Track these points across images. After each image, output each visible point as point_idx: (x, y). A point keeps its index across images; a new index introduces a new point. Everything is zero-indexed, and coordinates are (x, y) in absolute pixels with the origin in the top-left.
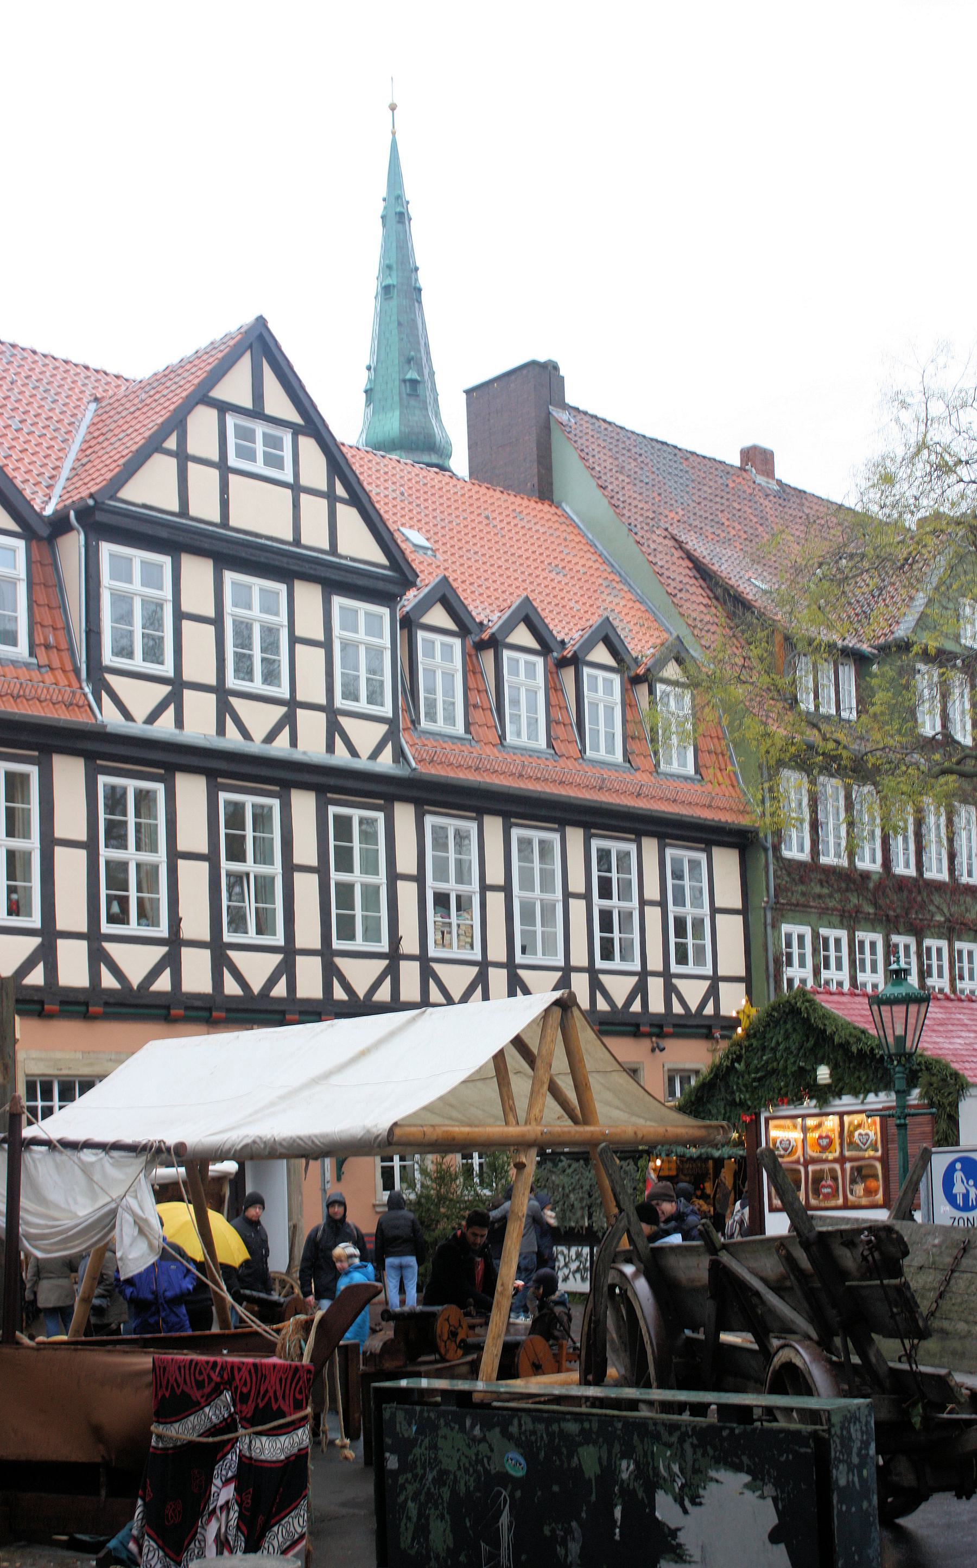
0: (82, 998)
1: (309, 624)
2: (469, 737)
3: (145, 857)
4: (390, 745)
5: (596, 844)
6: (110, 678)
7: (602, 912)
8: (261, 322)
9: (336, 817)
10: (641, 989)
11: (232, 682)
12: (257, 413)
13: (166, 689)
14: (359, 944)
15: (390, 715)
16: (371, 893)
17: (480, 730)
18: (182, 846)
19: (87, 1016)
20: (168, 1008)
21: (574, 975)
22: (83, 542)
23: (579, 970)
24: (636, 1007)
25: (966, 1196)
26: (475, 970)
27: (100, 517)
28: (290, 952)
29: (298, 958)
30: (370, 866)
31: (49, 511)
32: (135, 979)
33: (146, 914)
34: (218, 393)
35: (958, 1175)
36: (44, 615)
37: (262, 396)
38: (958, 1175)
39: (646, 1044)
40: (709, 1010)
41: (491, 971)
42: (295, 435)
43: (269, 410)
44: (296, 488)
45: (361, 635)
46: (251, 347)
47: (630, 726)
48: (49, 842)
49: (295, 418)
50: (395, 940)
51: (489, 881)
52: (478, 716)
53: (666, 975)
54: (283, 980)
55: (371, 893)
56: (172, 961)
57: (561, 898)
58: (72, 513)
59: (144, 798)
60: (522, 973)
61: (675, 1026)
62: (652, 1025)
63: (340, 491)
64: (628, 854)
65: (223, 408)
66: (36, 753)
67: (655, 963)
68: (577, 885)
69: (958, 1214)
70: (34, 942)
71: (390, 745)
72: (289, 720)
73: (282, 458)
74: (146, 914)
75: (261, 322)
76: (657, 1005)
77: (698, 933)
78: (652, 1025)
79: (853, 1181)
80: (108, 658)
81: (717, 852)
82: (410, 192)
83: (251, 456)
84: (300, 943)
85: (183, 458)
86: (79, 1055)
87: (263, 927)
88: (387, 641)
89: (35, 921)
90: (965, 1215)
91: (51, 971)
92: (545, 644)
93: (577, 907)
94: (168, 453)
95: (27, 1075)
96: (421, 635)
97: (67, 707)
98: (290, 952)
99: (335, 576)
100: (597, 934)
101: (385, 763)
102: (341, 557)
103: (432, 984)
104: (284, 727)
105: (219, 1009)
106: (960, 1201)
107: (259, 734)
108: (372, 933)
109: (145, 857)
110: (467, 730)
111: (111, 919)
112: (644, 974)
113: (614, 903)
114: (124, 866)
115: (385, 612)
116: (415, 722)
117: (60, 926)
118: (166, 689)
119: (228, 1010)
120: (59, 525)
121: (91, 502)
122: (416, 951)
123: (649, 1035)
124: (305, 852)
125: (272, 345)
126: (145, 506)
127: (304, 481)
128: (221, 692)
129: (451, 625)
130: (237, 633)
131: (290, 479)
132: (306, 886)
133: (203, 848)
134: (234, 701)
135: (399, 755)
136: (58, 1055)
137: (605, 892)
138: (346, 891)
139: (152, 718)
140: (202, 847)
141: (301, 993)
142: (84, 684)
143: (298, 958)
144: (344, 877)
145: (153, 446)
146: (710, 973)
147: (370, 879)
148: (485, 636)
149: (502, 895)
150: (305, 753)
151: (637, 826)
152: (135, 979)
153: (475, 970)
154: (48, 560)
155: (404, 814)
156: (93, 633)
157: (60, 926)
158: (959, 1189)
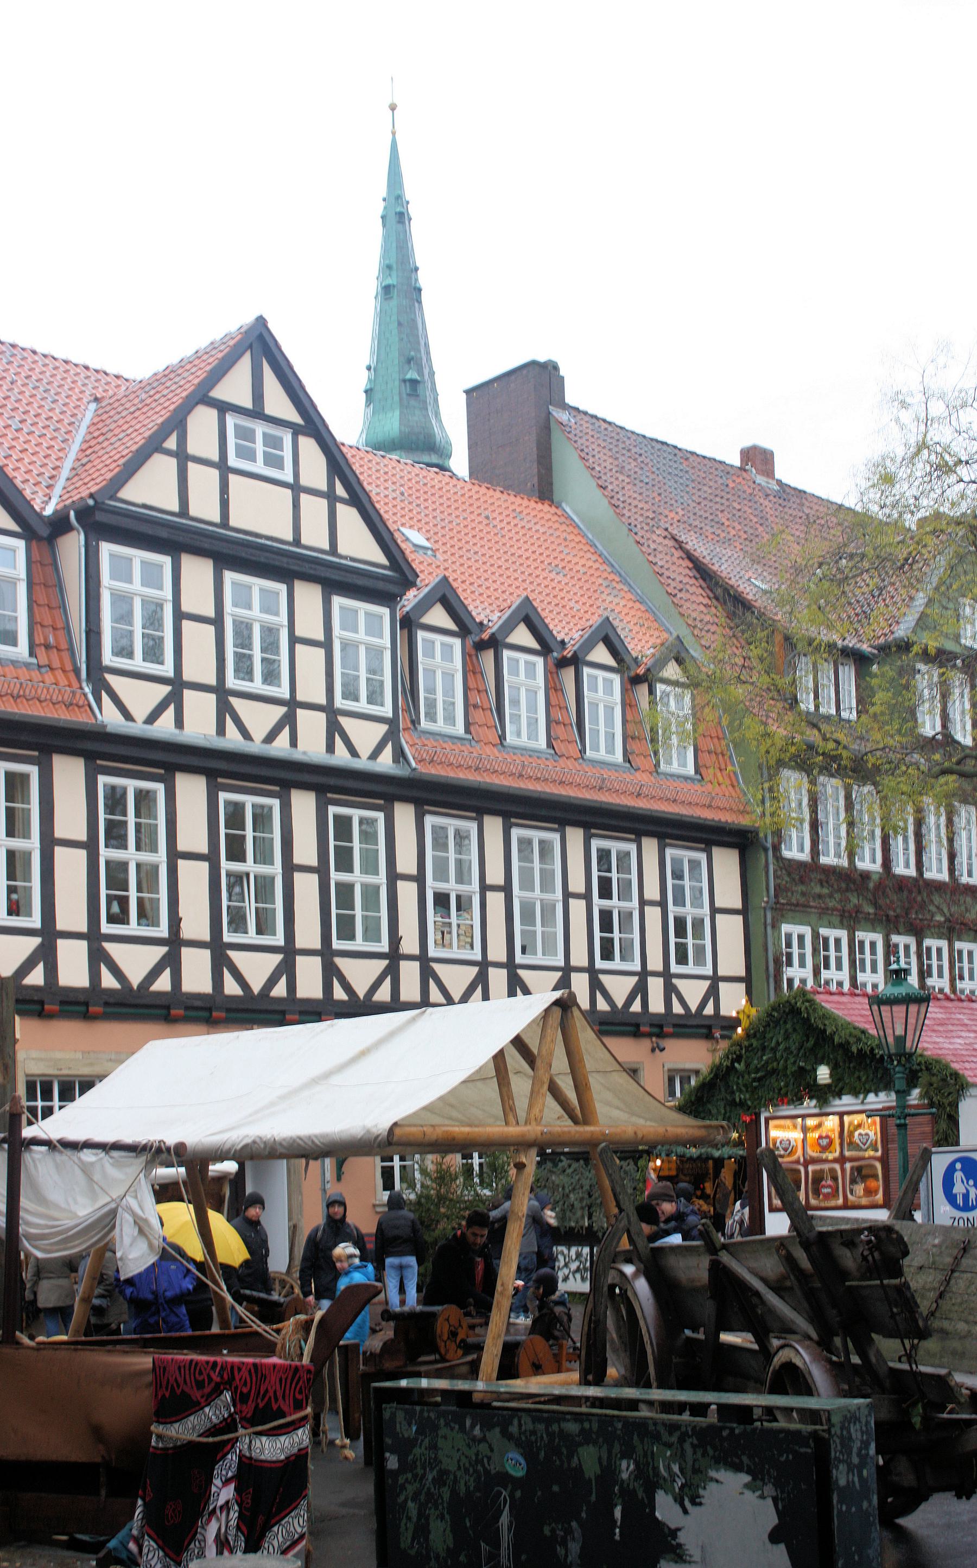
0: (82, 998)
1: (309, 624)
2: (469, 737)
3: (145, 857)
4: (390, 745)
5: (596, 844)
6: (110, 678)
7: (602, 912)
8: (261, 322)
9: (336, 817)
10: (641, 989)
11: (232, 682)
12: (257, 413)
13: (166, 689)
14: (359, 944)
15: (390, 715)
16: (371, 893)
17: (480, 730)
18: (182, 846)
19: (87, 1016)
20: (168, 1008)
21: (574, 975)
22: (83, 542)
23: (579, 970)
24: (636, 1007)
25: (966, 1196)
26: (475, 970)
27: (100, 517)
28: (290, 952)
29: (298, 958)
30: (370, 866)
31: (49, 511)
32: (135, 979)
33: (146, 914)
34: (218, 393)
35: (958, 1175)
36: (44, 615)
37: (262, 396)
38: (958, 1175)
39: (646, 1044)
40: (709, 1010)
41: (491, 971)
42: (295, 435)
43: (269, 410)
44: (296, 488)
45: (361, 635)
46: (251, 347)
47: (630, 726)
48: (49, 842)
49: (295, 418)
50: (395, 940)
51: (489, 881)
52: (478, 716)
53: (666, 975)
54: (283, 980)
55: (371, 893)
56: (172, 961)
57: (561, 898)
58: (72, 513)
59: (144, 798)
60: (522, 973)
61: (675, 1026)
62: (652, 1025)
63: (340, 491)
64: (628, 854)
65: (223, 408)
66: (36, 753)
67: (655, 963)
68: (577, 885)
69: (958, 1214)
70: (34, 942)
71: (390, 745)
72: (289, 720)
73: (282, 458)
74: (146, 914)
75: (261, 322)
76: (657, 1005)
77: (698, 933)
78: (652, 1025)
79: (853, 1181)
80: (108, 658)
81: (717, 852)
82: (410, 192)
83: (251, 456)
84: (300, 943)
85: (183, 458)
86: (79, 1055)
87: (263, 927)
88: (387, 641)
89: (35, 921)
90: (965, 1215)
91: (51, 971)
92: (545, 644)
93: (577, 907)
94: (168, 453)
95: (27, 1075)
96: (421, 635)
97: (67, 707)
98: (290, 952)
99: (335, 576)
100: (597, 934)
101: (385, 763)
102: (341, 557)
103: (432, 984)
104: (284, 727)
105: (219, 1009)
106: (960, 1201)
107: (259, 734)
108: (372, 933)
109: (145, 857)
110: (467, 730)
111: (111, 919)
112: (644, 974)
113: (614, 903)
114: (124, 866)
115: (385, 612)
116: (415, 722)
117: (60, 926)
118: (166, 689)
119: (228, 1010)
120: (59, 525)
121: (91, 502)
122: (416, 951)
123: (649, 1035)
124: (305, 852)
125: (272, 345)
126: (145, 506)
127: (304, 481)
128: (221, 692)
129: (451, 625)
130: (237, 633)
131: (290, 479)
132: (306, 886)
133: (203, 848)
134: (234, 701)
135: (399, 755)
136: (58, 1055)
137: (605, 892)
138: (346, 891)
139: (152, 718)
140: (202, 847)
141: (301, 993)
142: (84, 684)
143: (298, 958)
144: (344, 877)
145: (153, 446)
146: (710, 973)
147: (370, 879)
148: (485, 636)
149: (502, 895)
150: (305, 753)
151: (637, 826)
152: (135, 979)
153: (475, 970)
154: (48, 560)
155: (404, 814)
156: (93, 633)
157: (60, 926)
158: (959, 1189)
